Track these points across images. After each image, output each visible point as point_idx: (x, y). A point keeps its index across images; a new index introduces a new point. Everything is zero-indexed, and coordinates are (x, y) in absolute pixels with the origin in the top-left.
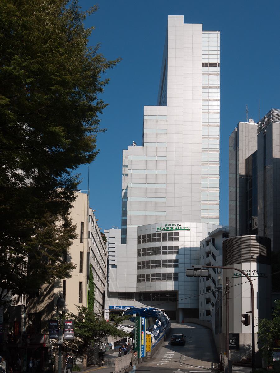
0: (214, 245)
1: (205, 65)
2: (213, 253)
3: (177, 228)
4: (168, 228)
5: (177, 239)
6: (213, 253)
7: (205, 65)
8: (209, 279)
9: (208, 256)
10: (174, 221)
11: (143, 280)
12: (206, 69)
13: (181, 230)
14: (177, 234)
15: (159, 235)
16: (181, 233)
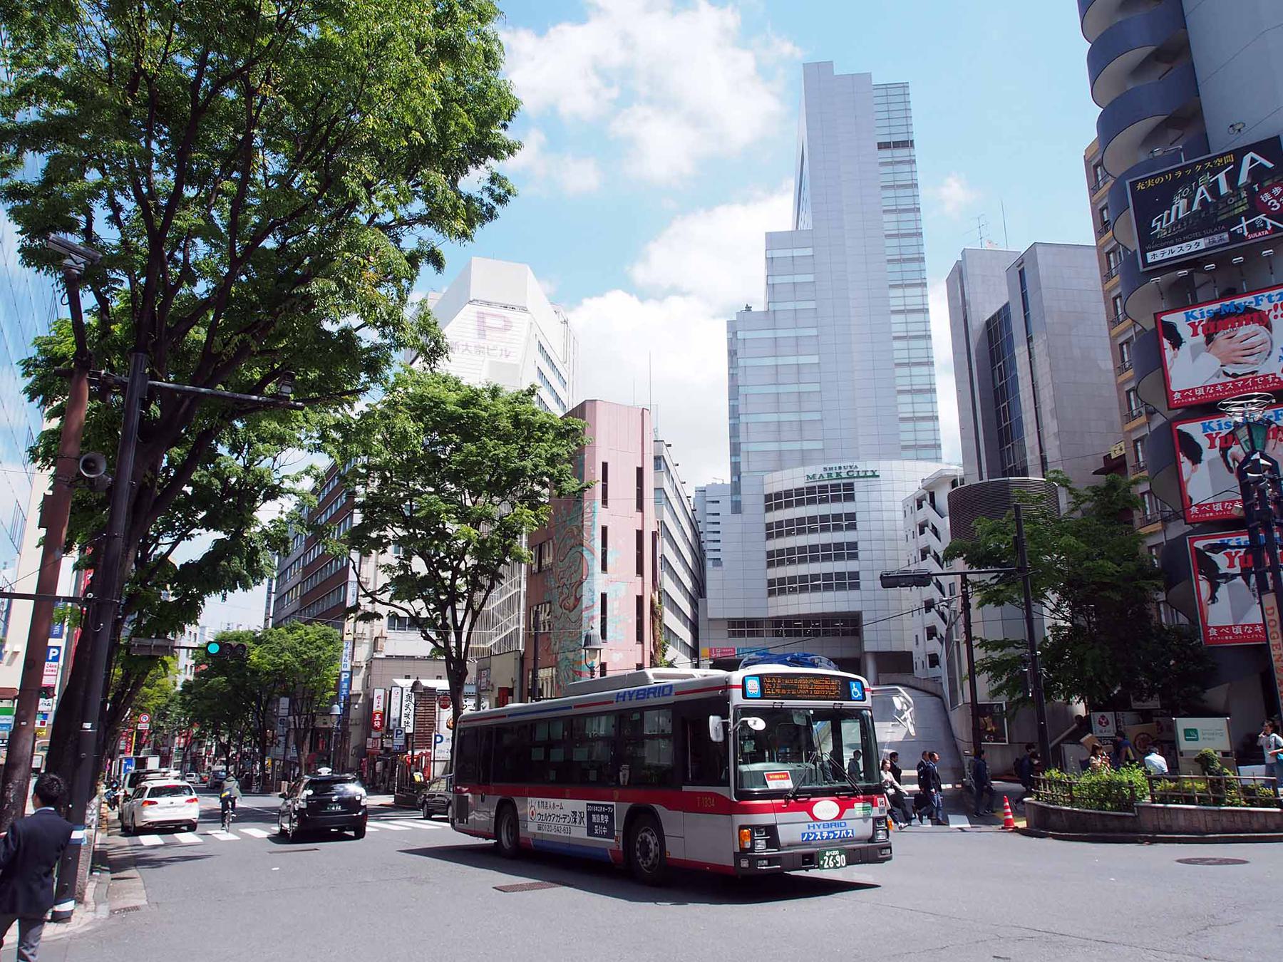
0: (934, 507)
1: (882, 146)
2: (933, 525)
3: (850, 474)
4: (830, 475)
5: (850, 498)
6: (935, 552)
7: (882, 146)
8: (932, 609)
9: (922, 532)
10: (842, 459)
11: (782, 591)
12: (887, 153)
13: (858, 477)
14: (850, 487)
15: (811, 490)
16: (859, 485)
